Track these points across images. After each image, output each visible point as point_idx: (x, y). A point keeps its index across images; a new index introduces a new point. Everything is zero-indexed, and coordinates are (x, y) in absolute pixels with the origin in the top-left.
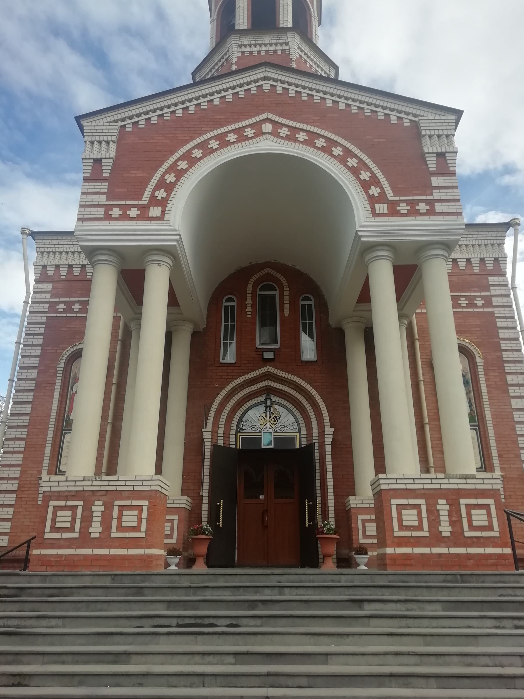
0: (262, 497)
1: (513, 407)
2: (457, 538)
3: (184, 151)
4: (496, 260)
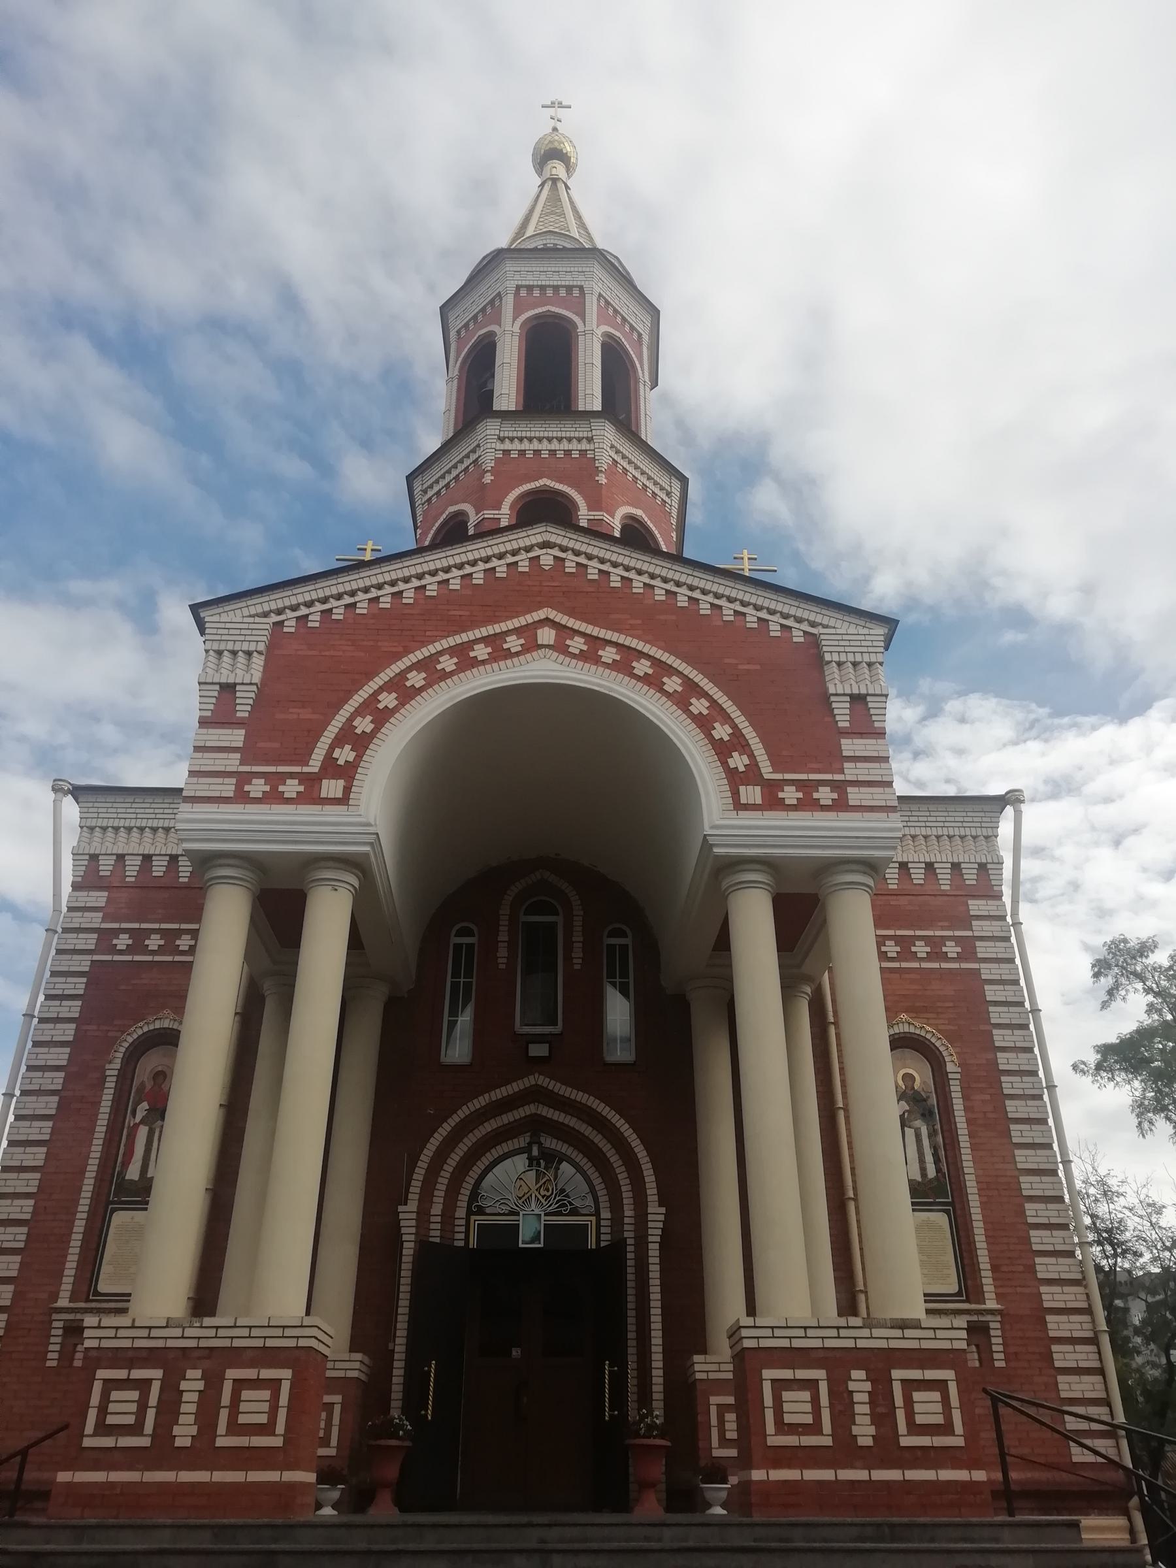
0: (516, 1353)
1: (1020, 1166)
2: (886, 1451)
3: (392, 675)
4: (982, 867)
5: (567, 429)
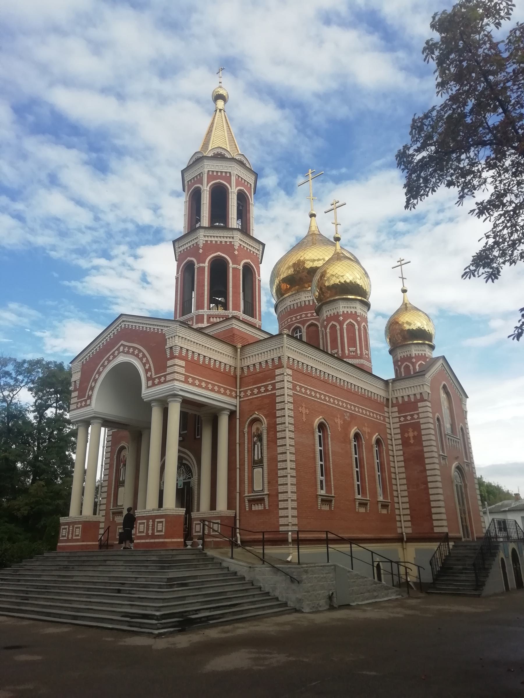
5: (226, 233)
